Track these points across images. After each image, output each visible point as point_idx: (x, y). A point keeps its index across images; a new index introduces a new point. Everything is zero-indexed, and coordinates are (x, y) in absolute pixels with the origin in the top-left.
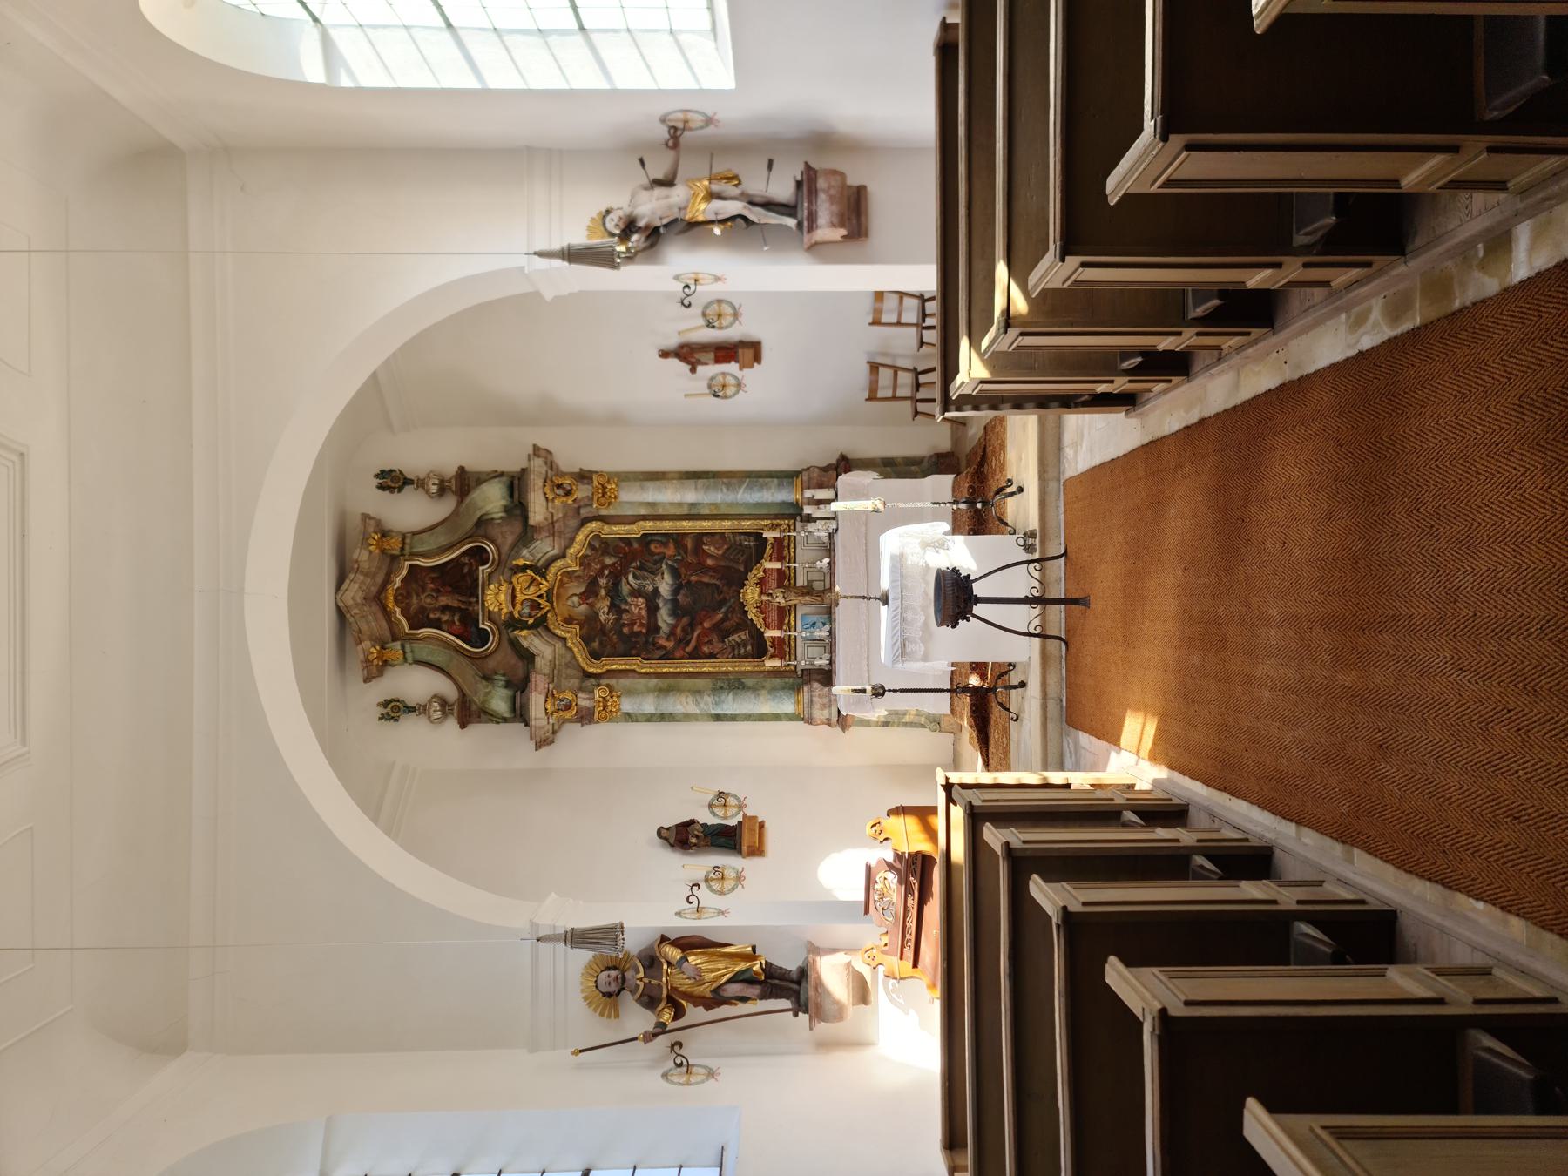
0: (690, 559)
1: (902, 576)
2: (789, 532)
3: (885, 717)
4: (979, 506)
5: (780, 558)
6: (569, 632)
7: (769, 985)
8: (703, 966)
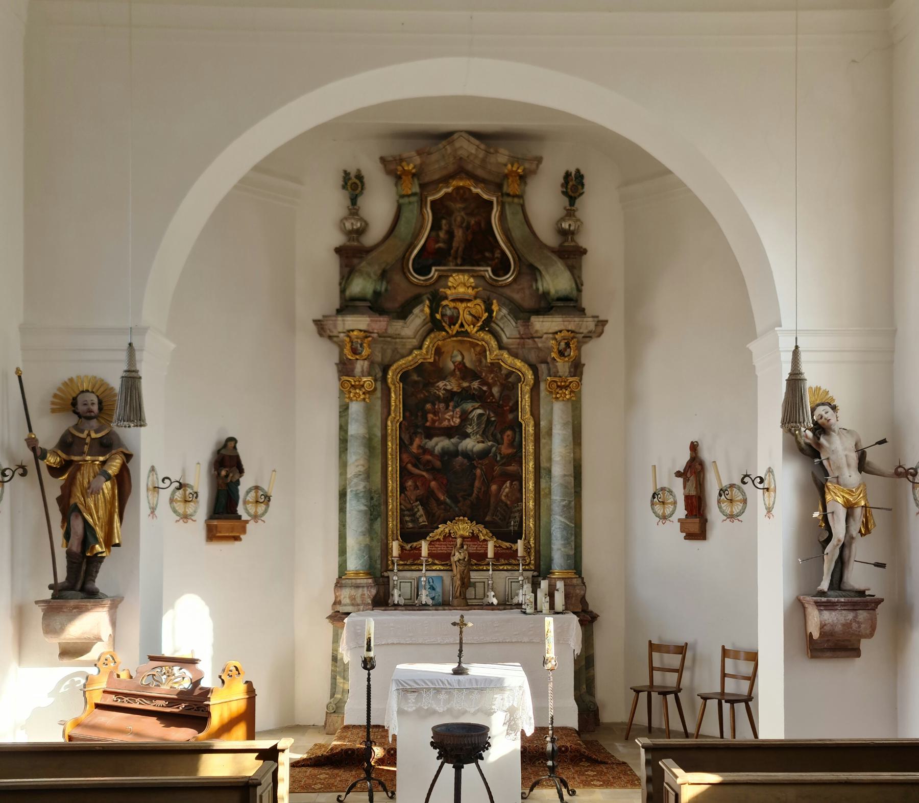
0: (497, 469)
1: (482, 689)
2: (523, 565)
3: (342, 659)
5: (497, 556)
6: (427, 352)
8: (100, 496)
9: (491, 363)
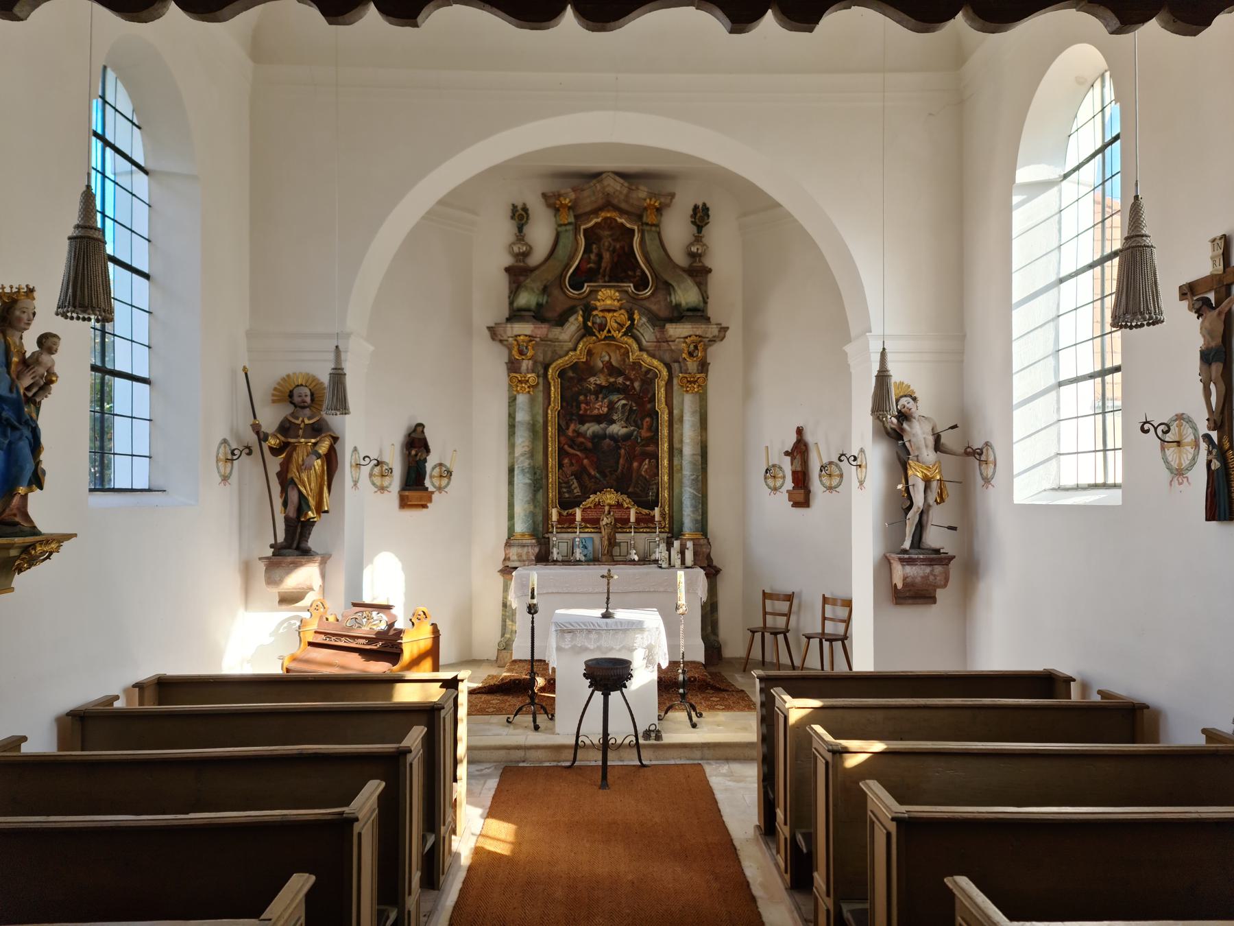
0: (638, 449)
2: (659, 528)
3: (511, 605)
4: (681, 691)
5: (638, 521)
6: (580, 353)
7: (296, 524)
8: (312, 472)
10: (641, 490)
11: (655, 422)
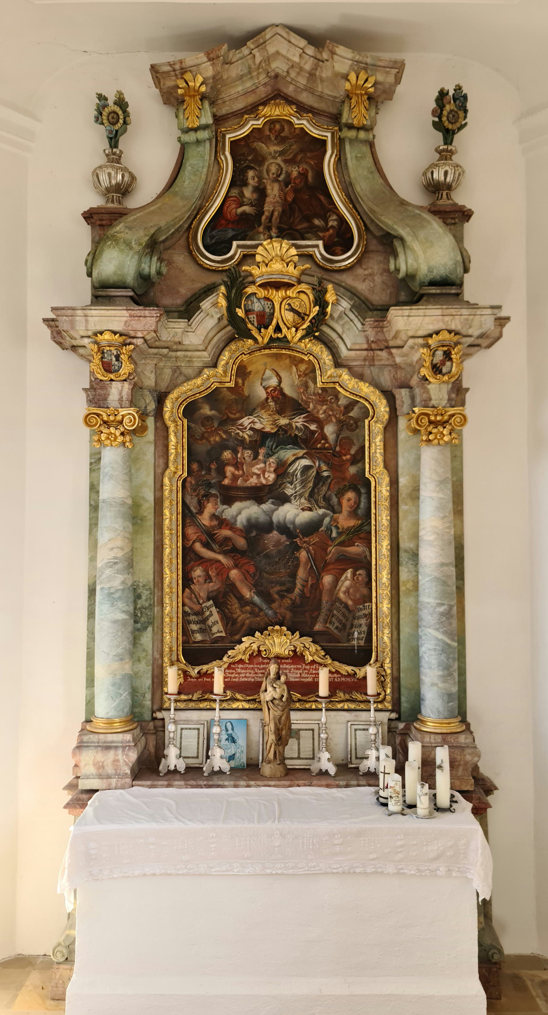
0: (332, 550)
5: (333, 687)
6: (225, 372)
9: (323, 389)
10: (337, 628)
11: (363, 500)
